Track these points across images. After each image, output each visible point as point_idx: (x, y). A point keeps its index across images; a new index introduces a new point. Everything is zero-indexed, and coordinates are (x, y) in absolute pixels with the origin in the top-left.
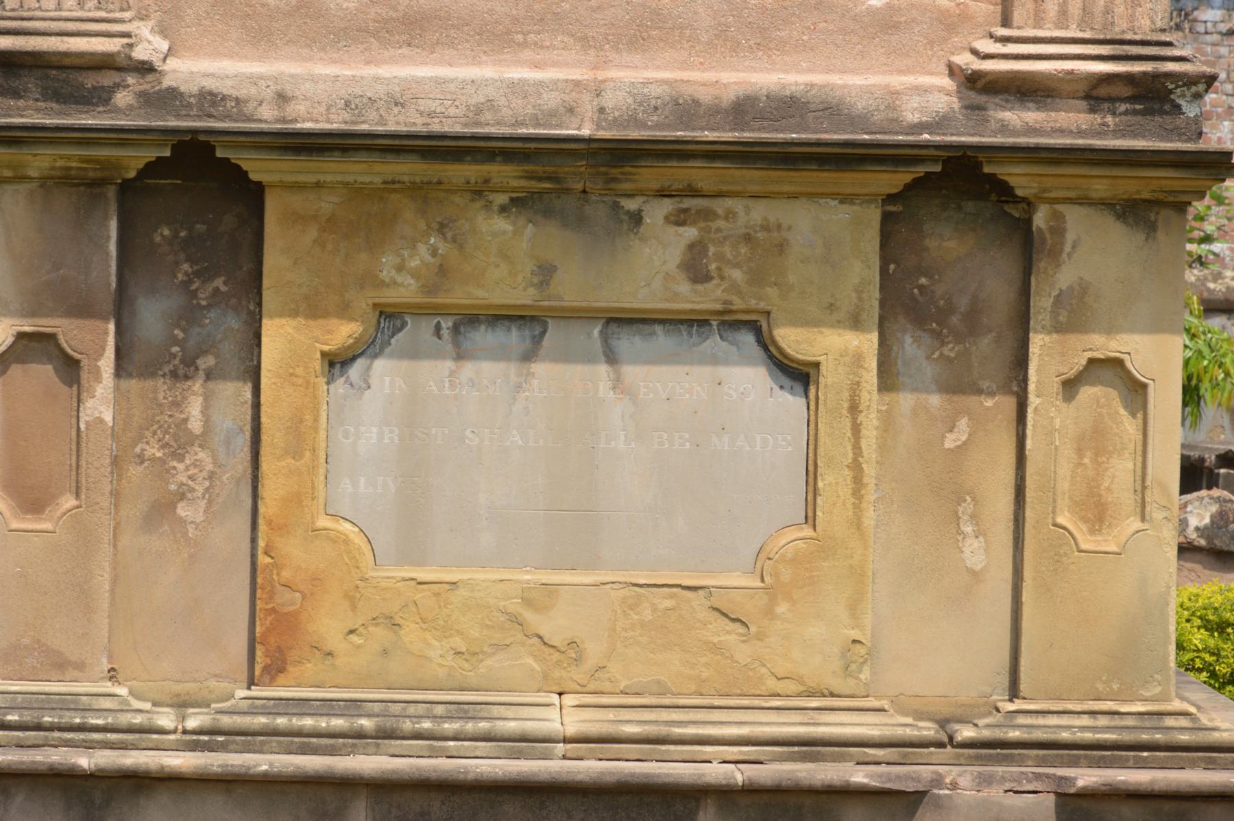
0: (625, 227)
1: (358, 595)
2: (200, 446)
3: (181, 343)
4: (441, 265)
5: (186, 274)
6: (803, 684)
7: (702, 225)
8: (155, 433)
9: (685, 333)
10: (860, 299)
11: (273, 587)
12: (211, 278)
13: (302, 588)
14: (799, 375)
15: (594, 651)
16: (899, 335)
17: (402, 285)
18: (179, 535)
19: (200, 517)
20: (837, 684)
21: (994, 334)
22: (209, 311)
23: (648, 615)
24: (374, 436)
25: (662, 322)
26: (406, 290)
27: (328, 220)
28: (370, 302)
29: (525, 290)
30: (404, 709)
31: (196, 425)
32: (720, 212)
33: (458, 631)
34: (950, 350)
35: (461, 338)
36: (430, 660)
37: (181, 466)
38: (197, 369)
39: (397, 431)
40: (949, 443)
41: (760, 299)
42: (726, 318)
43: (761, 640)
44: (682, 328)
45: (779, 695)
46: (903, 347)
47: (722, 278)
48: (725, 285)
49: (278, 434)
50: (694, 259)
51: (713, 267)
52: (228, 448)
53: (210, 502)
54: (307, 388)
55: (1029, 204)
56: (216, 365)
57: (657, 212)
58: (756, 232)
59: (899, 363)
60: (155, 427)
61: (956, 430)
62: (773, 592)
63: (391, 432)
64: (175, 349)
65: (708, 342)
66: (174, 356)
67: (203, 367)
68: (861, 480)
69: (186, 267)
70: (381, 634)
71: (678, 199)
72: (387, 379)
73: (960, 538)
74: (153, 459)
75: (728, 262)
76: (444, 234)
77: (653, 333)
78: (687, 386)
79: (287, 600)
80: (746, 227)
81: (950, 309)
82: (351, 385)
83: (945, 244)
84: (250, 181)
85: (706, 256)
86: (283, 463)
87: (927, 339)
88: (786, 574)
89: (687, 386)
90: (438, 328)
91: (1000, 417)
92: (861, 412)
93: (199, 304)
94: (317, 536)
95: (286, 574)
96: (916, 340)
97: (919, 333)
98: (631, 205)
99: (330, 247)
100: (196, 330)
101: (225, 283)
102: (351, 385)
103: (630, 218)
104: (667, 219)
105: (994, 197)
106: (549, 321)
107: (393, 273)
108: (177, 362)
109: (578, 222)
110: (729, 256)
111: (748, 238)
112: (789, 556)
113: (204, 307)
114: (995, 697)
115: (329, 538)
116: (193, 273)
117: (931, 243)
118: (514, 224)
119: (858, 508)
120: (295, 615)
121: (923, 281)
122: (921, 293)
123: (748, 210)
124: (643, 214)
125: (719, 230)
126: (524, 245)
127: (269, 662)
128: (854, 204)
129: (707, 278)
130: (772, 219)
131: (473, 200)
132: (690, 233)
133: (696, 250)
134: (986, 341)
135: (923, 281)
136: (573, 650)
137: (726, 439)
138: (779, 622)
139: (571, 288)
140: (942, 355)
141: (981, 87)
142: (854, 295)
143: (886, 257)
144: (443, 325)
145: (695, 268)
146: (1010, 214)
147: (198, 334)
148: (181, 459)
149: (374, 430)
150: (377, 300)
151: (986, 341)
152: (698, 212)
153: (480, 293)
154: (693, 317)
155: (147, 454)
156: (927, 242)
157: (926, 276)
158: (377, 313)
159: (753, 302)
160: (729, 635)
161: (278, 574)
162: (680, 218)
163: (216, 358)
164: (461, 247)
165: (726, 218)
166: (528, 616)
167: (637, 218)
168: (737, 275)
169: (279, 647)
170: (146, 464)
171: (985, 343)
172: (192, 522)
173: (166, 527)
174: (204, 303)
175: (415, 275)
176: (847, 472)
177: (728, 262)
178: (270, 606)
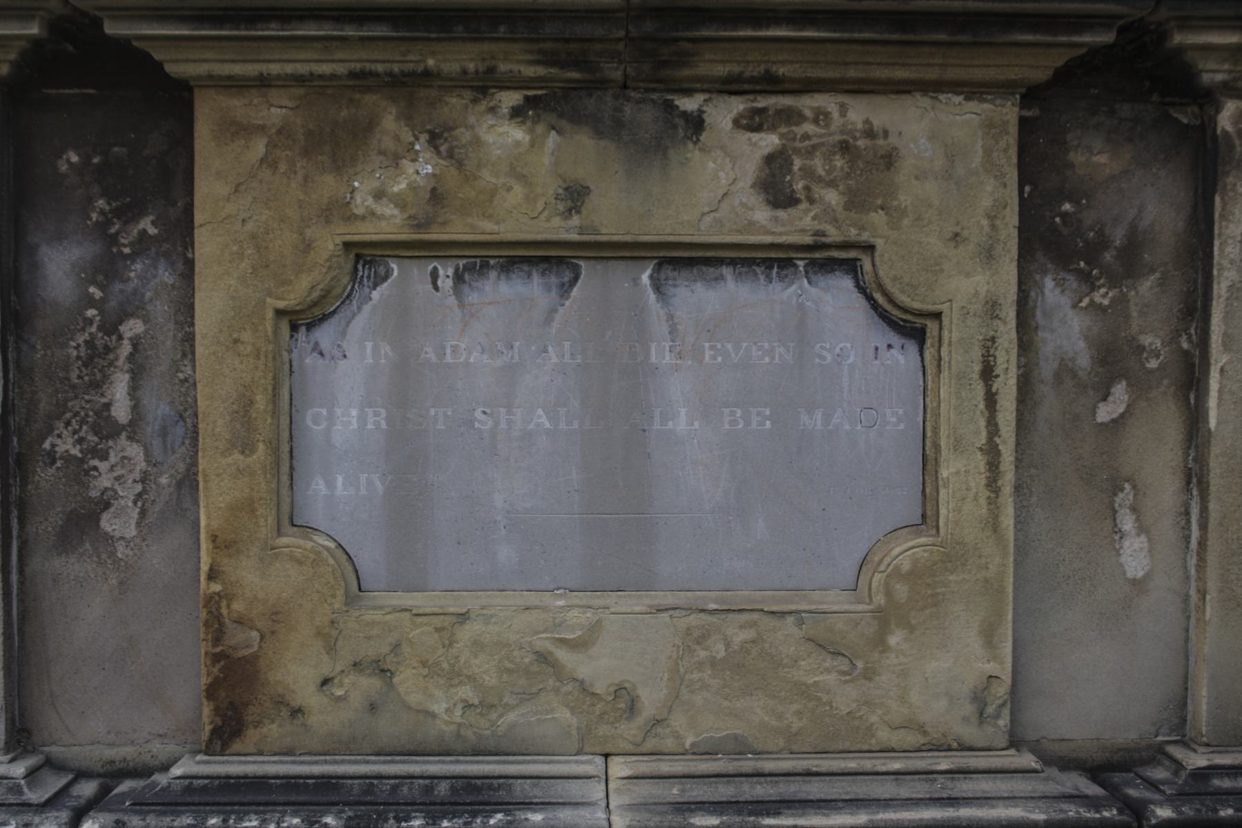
0: (681, 133)
1: (334, 633)
2: (129, 438)
3: (99, 305)
4: (434, 190)
5: (102, 212)
6: (925, 733)
7: (783, 130)
8: (68, 424)
9: (762, 277)
10: (993, 227)
11: (221, 624)
12: (135, 219)
13: (260, 624)
14: (912, 327)
15: (651, 699)
16: (1038, 277)
17: (381, 217)
18: (104, 556)
19: (131, 532)
20: (971, 733)
21: (1157, 275)
22: (134, 261)
23: (720, 651)
24: (354, 421)
25: (733, 262)
26: (389, 223)
27: (279, 132)
28: (338, 240)
29: (548, 220)
30: (395, 788)
31: (121, 412)
32: (808, 113)
33: (469, 677)
34: (1103, 296)
35: (466, 288)
36: (433, 716)
37: (103, 466)
38: (120, 338)
39: (383, 412)
40: (1105, 413)
41: (863, 228)
42: (817, 255)
43: (870, 679)
44: (758, 270)
45: (893, 750)
46: (1042, 292)
47: (811, 201)
48: (816, 210)
49: (220, 422)
50: (774, 176)
51: (799, 186)
52: (164, 441)
53: (143, 513)
54: (258, 357)
55: (1209, 99)
56: (146, 331)
57: (723, 113)
58: (855, 139)
59: (1039, 313)
60: (68, 415)
61: (1111, 398)
62: (885, 619)
63: (376, 414)
64: (91, 313)
65: (793, 288)
66: (90, 322)
67: (128, 335)
68: (997, 467)
69: (101, 203)
70: (370, 683)
71: (751, 97)
72: (369, 345)
73: (1117, 537)
74: (68, 458)
75: (820, 180)
76: (436, 148)
77: (721, 278)
78: (766, 345)
79: (243, 640)
80: (842, 132)
81: (1103, 243)
82: (321, 354)
83: (1095, 159)
84: (167, 75)
85: (790, 171)
86: (230, 460)
87: (1072, 282)
88: (901, 591)
89: (766, 345)
90: (434, 275)
91: (1166, 382)
92: (997, 376)
93: (121, 253)
94: (277, 555)
95: (238, 606)
96: (1059, 283)
97: (1062, 275)
98: (688, 104)
99: (283, 167)
100: (118, 286)
101: (153, 223)
102: (321, 354)
103: (687, 121)
104: (736, 123)
105: (1155, 98)
106: (582, 263)
107: (370, 201)
108: (94, 329)
109: (611, 129)
110: (821, 171)
111: (845, 148)
112: (906, 567)
113: (127, 257)
114: (1160, 738)
115: (292, 558)
116: (111, 211)
117: (1077, 158)
118: (531, 131)
119: (993, 503)
120: (253, 660)
121: (1067, 207)
122: (1064, 222)
123: (843, 109)
124: (705, 116)
125: (806, 137)
126: (546, 160)
127: (220, 723)
128: (985, 101)
129: (792, 201)
130: (877, 123)
131: (475, 101)
132: (769, 141)
133: (776, 162)
134: (1149, 284)
135: (1067, 207)
136: (625, 700)
137: (818, 415)
138: (893, 656)
139: (614, 211)
140: (1092, 303)
142: (985, 222)
143: (1024, 178)
144: (441, 272)
145: (776, 187)
146: (1177, 120)
147: (121, 291)
148: (104, 457)
149: (354, 413)
150: (348, 238)
151: (1149, 284)
152: (779, 112)
153: (489, 226)
154: (773, 255)
155: (60, 449)
156: (1072, 156)
157: (1070, 201)
158: (352, 256)
159: (853, 231)
160: (822, 674)
161: (228, 607)
162: (753, 122)
163: (145, 322)
164: (460, 165)
165: (816, 121)
166: (562, 655)
167: (696, 123)
168: (832, 197)
169: (231, 703)
170: (58, 464)
171: (1147, 286)
172: (122, 538)
173: (88, 546)
174: (127, 250)
175: (400, 202)
176: (979, 455)
177: (820, 180)
178: (219, 649)
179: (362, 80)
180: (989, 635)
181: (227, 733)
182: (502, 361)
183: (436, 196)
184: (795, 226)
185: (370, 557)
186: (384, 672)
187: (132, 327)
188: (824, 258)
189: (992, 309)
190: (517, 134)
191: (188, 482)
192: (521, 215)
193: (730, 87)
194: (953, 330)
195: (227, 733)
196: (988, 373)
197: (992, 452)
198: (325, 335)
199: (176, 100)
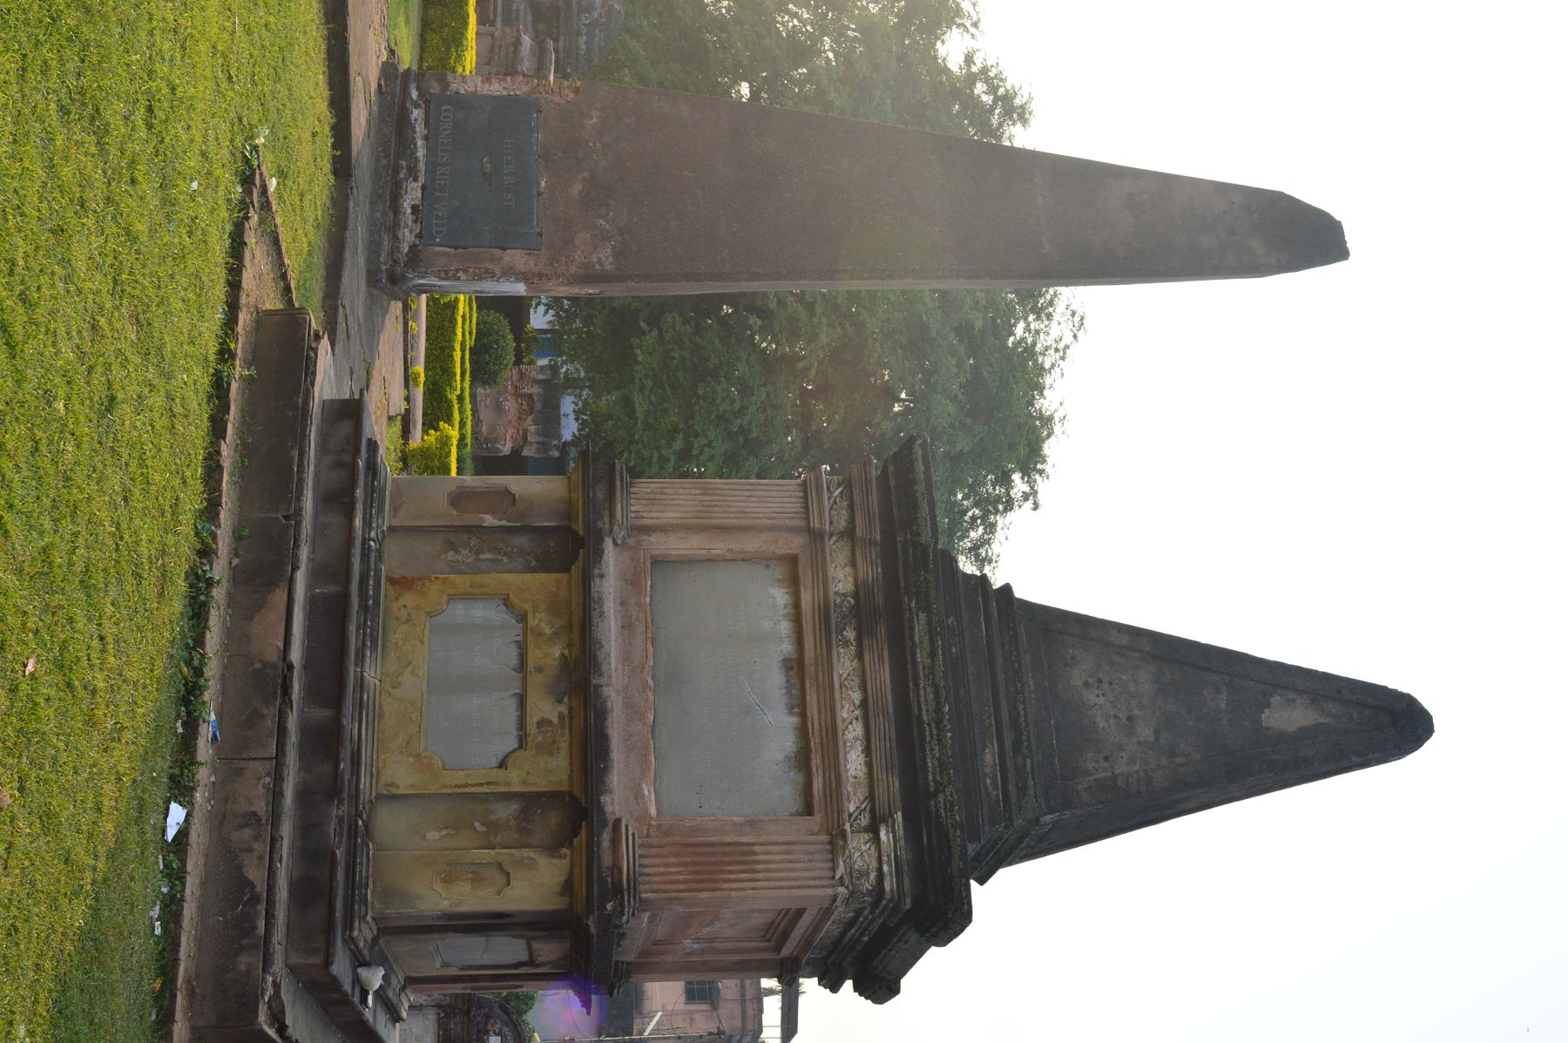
14: (502, 765)
15: (397, 692)
20: (382, 782)
31: (482, 556)
34: (512, 822)
40: (477, 824)
57: (563, 708)
132: (556, 721)
133: (550, 723)
139: (535, 680)
141: (618, 821)
145: (543, 723)
162: (561, 717)
167: (560, 702)
179: (571, 613)
180: (412, 786)
181: (392, 581)
182: (494, 653)
183: (540, 634)
184: (531, 728)
185: (440, 619)
186: (407, 622)
187: (505, 559)
188: (522, 741)
189: (508, 784)
190: (557, 655)
191: (462, 572)
192: (534, 656)
193: (571, 710)
194: (501, 772)
195: (392, 581)
196: (489, 783)
197: (466, 785)
198: (502, 607)
199: (567, 570)
